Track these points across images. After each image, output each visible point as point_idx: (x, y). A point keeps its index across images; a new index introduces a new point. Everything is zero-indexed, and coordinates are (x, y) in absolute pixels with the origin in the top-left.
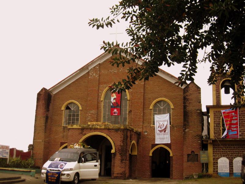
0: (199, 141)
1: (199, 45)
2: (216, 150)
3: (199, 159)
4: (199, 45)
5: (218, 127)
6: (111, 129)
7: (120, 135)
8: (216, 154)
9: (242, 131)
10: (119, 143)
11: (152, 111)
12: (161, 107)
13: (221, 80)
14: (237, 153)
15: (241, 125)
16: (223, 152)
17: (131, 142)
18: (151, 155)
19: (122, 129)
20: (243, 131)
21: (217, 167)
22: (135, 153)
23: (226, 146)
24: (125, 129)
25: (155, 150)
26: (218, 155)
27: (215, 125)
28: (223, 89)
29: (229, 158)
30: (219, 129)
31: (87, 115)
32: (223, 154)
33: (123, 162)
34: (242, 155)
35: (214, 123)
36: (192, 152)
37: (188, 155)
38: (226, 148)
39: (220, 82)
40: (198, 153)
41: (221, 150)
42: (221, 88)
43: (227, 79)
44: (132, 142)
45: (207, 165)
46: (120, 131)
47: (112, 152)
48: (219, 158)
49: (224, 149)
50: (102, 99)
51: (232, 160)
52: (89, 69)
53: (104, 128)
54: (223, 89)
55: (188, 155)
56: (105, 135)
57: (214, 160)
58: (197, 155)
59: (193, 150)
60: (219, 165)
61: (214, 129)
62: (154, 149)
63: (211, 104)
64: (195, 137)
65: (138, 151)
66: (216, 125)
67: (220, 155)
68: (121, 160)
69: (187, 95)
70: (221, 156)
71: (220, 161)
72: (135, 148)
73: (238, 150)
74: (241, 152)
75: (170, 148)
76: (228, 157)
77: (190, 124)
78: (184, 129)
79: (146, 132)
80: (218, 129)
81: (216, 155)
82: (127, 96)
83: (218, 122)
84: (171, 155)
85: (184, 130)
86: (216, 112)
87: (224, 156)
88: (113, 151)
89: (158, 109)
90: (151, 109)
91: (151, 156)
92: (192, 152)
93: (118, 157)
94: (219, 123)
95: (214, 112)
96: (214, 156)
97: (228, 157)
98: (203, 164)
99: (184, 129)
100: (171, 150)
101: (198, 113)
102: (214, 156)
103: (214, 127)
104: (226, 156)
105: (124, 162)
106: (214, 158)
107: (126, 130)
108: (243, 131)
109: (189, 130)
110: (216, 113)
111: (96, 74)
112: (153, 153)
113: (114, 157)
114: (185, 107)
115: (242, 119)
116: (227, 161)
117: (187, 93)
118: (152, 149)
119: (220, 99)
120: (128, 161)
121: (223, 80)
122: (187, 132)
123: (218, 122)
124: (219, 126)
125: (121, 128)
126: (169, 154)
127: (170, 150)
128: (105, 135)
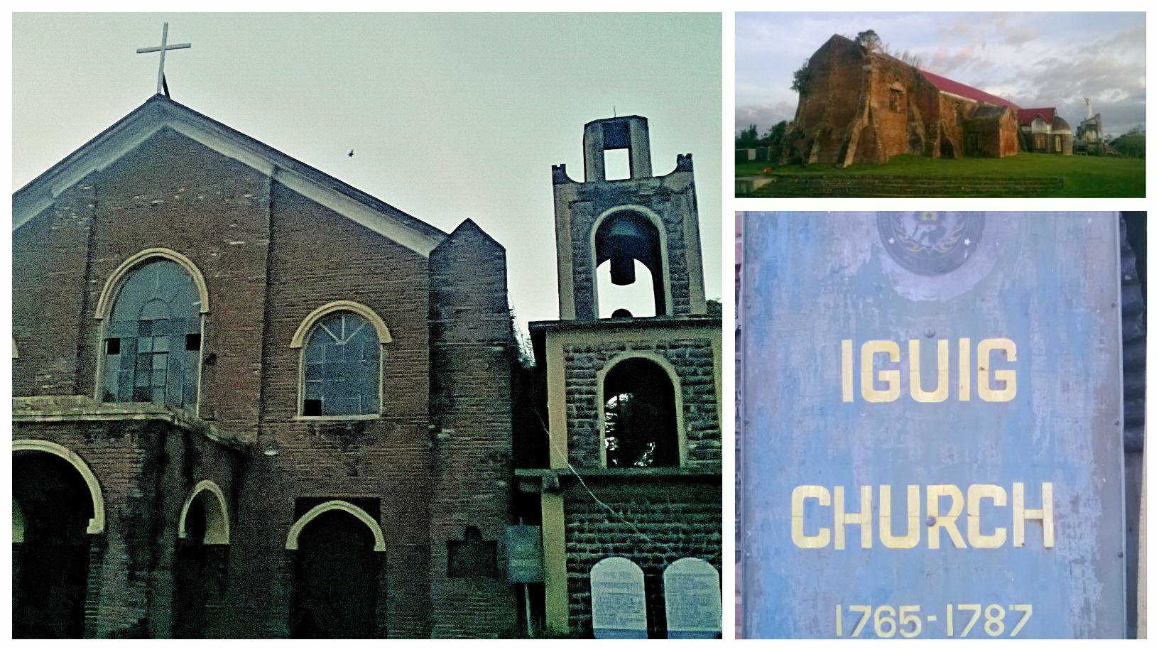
0: (502, 483)
1: (616, 415)
2: (582, 521)
3: (500, 566)
4: (616, 415)
5: (587, 416)
6: (94, 422)
7: (133, 452)
8: (579, 541)
9: (701, 434)
10: (128, 488)
11: (302, 352)
12: (340, 338)
13: (595, 215)
14: (682, 536)
15: (693, 408)
16: (611, 531)
17: (190, 484)
18: (292, 544)
19: (137, 422)
20: (705, 437)
21: (588, 601)
22: (219, 535)
23: (628, 505)
24: (151, 422)
25: (311, 522)
26: (588, 546)
27: (569, 409)
28: (607, 265)
29: (645, 560)
30: (592, 425)
31: (40, 379)
32: (612, 541)
33: (137, 579)
34: (704, 545)
35: (568, 401)
36: (472, 531)
37: (452, 545)
38: (625, 512)
39: (592, 223)
40: (495, 537)
41: (601, 521)
42: (599, 262)
43: (623, 208)
44: (199, 488)
45: (538, 590)
46: (133, 432)
47: (89, 531)
48: (595, 561)
49: (619, 521)
50: (98, 316)
51: (661, 572)
52: (56, 195)
53: (59, 419)
54: (607, 265)
55: (452, 545)
56: (67, 451)
57: (569, 570)
58: (493, 544)
59: (475, 522)
60: (595, 594)
61: (570, 425)
62: (304, 517)
63: (551, 313)
64: (482, 462)
65: (234, 520)
66: (575, 412)
67: (599, 545)
68: (130, 567)
69: (446, 283)
70: (605, 550)
71: (597, 573)
72: (219, 510)
73: (685, 526)
74: (697, 531)
75: (376, 515)
76: (636, 554)
77: (463, 404)
78: (432, 427)
79: (276, 446)
80: (586, 426)
81: (582, 546)
82: (198, 299)
83: (584, 396)
84: (380, 546)
85: (432, 431)
86: (577, 351)
87: (617, 552)
88: (95, 526)
89: (329, 347)
90: (297, 350)
91: (292, 552)
92: (472, 531)
93: (117, 552)
94: (591, 401)
95: (567, 351)
96: (569, 550)
97: (636, 554)
98: (519, 587)
99: (432, 427)
100: (379, 522)
101: (493, 354)
102: (569, 550)
103: (569, 416)
104: (630, 550)
105: (143, 579)
106: (570, 561)
107: (155, 431)
108: (705, 437)
109: (452, 431)
110: (576, 355)
111: (81, 214)
112: (302, 538)
113: (100, 556)
114: (436, 331)
115: (700, 382)
116: (637, 574)
117: (449, 274)
118: (297, 517)
119: (592, 296)
120: (168, 576)
121: (604, 215)
122: (446, 440)
123: (584, 396)
124: (593, 413)
125: (137, 418)
126: (371, 538)
127: (374, 521)
128: (62, 452)
